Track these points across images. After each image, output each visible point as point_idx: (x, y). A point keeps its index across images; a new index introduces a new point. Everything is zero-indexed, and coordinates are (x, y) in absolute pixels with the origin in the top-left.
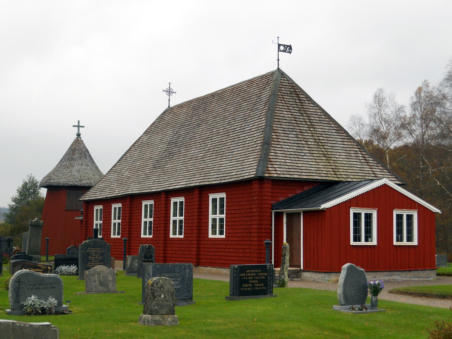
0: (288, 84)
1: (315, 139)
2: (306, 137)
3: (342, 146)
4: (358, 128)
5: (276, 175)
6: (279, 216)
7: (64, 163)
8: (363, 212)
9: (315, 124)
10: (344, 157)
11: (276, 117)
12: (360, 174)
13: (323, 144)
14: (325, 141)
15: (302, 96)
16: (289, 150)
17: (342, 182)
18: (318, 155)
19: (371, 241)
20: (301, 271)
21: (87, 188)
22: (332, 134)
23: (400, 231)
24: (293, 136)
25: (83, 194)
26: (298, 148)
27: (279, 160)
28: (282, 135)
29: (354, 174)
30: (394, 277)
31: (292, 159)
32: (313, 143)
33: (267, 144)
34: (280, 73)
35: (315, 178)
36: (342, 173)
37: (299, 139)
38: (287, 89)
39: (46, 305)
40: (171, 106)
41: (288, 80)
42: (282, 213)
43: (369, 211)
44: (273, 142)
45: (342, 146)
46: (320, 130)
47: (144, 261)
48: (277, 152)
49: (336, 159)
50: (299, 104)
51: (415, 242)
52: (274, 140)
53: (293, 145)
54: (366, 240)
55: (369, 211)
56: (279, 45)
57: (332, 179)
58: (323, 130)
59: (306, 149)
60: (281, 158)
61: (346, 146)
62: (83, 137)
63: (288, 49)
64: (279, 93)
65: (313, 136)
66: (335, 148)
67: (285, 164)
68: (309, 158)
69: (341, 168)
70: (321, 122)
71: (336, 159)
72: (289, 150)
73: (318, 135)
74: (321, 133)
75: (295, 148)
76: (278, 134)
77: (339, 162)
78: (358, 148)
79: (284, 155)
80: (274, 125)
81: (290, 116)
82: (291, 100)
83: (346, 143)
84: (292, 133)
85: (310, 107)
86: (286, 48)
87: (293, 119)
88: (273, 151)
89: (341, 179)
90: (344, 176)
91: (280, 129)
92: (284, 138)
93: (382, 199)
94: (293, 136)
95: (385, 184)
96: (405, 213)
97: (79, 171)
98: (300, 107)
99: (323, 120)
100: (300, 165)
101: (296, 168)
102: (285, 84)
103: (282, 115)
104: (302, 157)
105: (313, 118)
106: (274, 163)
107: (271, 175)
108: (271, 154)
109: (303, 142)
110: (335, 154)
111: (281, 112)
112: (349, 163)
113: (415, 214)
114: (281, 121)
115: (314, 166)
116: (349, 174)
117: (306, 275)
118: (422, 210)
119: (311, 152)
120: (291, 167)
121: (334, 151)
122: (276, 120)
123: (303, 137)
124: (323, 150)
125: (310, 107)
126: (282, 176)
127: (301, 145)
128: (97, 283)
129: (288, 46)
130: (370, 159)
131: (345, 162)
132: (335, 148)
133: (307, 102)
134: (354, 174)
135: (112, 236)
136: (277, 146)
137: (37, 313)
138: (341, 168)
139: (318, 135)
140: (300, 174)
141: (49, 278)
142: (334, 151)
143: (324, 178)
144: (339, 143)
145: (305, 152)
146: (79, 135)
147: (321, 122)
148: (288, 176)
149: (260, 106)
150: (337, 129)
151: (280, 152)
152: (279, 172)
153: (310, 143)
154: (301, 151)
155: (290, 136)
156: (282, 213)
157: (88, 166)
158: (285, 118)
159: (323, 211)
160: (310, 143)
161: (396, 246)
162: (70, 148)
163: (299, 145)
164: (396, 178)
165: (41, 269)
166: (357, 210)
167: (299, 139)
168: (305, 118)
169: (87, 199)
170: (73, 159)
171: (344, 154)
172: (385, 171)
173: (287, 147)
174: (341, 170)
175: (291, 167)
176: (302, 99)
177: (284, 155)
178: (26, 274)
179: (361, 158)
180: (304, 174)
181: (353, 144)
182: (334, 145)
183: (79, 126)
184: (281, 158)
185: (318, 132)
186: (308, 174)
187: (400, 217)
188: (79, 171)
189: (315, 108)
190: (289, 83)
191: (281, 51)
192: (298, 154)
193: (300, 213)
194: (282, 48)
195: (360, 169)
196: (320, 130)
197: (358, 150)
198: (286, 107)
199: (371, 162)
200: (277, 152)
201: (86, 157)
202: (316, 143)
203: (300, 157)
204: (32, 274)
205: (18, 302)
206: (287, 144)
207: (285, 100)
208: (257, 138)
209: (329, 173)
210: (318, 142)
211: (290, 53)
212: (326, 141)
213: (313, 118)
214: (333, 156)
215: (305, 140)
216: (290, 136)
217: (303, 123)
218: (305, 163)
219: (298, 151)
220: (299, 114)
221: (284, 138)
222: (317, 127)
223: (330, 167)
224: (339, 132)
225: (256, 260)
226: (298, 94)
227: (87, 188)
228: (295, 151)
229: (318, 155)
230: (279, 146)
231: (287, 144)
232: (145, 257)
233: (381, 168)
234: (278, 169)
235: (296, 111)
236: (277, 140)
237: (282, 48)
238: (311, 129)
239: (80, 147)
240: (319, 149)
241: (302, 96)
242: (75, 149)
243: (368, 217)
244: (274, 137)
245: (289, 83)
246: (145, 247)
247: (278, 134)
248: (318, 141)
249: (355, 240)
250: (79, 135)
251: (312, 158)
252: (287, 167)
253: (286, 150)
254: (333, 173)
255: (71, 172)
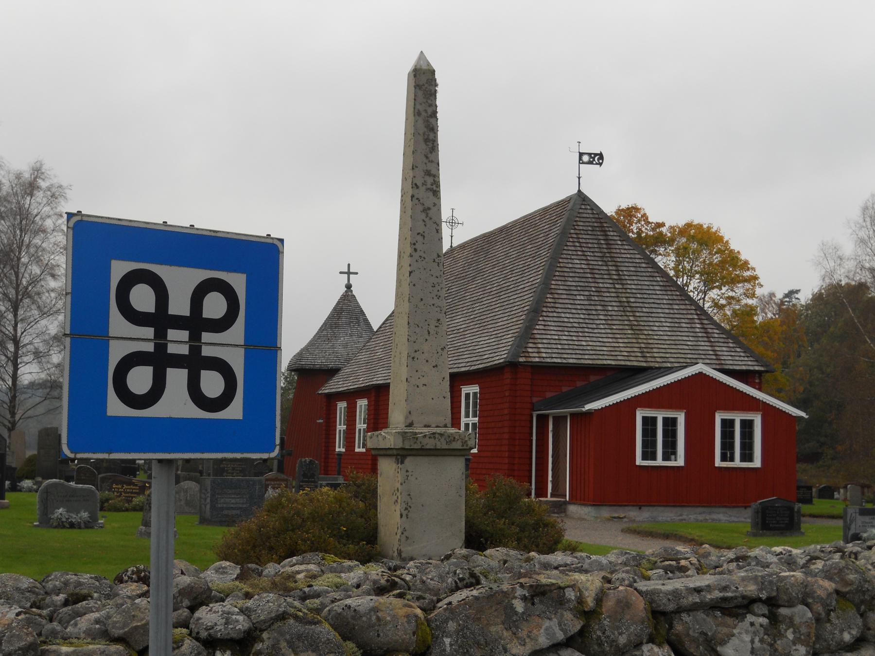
0: (591, 216)
1: (620, 302)
2: (606, 299)
3: (667, 311)
4: (832, 264)
5: (537, 360)
6: (543, 420)
7: (325, 333)
8: (660, 416)
9: (627, 277)
10: (667, 329)
11: (558, 269)
12: (689, 356)
13: (635, 309)
14: (638, 305)
15: (612, 234)
16: (571, 320)
17: (651, 368)
18: (621, 327)
19: (676, 460)
20: (565, 503)
21: (333, 372)
22: (654, 292)
23: (728, 446)
24: (582, 298)
25: (326, 381)
26: (587, 317)
27: (549, 337)
28: (565, 296)
29: (679, 355)
30: (715, 516)
31: (572, 334)
32: (616, 309)
33: (536, 311)
34: (581, 198)
35: (605, 362)
36: (656, 355)
37: (592, 303)
38: (587, 224)
39: (74, 518)
40: (454, 245)
41: (592, 209)
42: (546, 417)
43: (670, 414)
44: (545, 309)
45: (667, 311)
46: (633, 287)
47: (303, 482)
48: (549, 323)
49: (650, 333)
50: (605, 246)
51: (757, 463)
52: (548, 305)
53: (579, 312)
54: (666, 458)
55: (670, 414)
56: (581, 155)
57: (635, 364)
58: (640, 287)
59: (602, 317)
60: (553, 332)
61: (676, 311)
62: (355, 291)
63: (597, 158)
64: (572, 231)
65: (618, 297)
66: (653, 315)
67: (557, 342)
68: (603, 331)
69: (656, 346)
70: (639, 274)
71: (650, 333)
72: (571, 320)
73: (628, 295)
74: (634, 291)
75: (582, 316)
76: (556, 296)
77: (656, 337)
78: (697, 314)
79: (560, 329)
80: (553, 282)
81: (583, 266)
82: (591, 241)
83: (676, 307)
84: (582, 293)
85: (623, 251)
86: (594, 159)
87: (588, 271)
88: (543, 323)
89: (652, 365)
90: (658, 360)
91: (561, 287)
92: (567, 301)
93: (699, 397)
94: (582, 298)
95: (701, 373)
96: (738, 417)
97: (345, 346)
98: (606, 251)
99: (643, 270)
100: (584, 343)
101: (576, 347)
102: (585, 215)
103: (570, 266)
104: (590, 330)
105: (624, 269)
106: (539, 341)
107: (530, 360)
108: (537, 327)
109: (599, 308)
110: (651, 324)
111: (570, 261)
112: (673, 338)
113: (757, 420)
114: (566, 274)
115: (608, 344)
116: (668, 355)
117: (572, 509)
118: (769, 413)
119: (610, 322)
120: (566, 347)
121: (651, 319)
122: (557, 273)
123: (601, 298)
124: (631, 318)
125: (623, 251)
126: (549, 360)
127: (594, 312)
128: (183, 503)
129: (596, 155)
130: (715, 331)
131: (666, 338)
132: (653, 315)
133: (619, 242)
134: (679, 355)
135: (357, 450)
136: (551, 314)
137: (64, 527)
138: (656, 346)
139: (628, 295)
140: (580, 357)
141: (81, 489)
142: (651, 319)
143: (623, 363)
144: (663, 306)
145: (598, 322)
146: (349, 287)
147: (639, 274)
148: (559, 361)
149: (543, 252)
150: (665, 284)
151: (553, 324)
152: (544, 355)
153: (610, 308)
154: (591, 322)
155: (578, 297)
156: (546, 417)
157: (361, 337)
158: (573, 270)
159: (589, 413)
160: (610, 308)
161: (720, 468)
162: (335, 309)
163: (590, 312)
164: (757, 361)
165: (136, 485)
166: (650, 413)
167: (592, 303)
168: (610, 268)
169: (326, 391)
170: (337, 326)
171: (668, 324)
172: (738, 350)
173: (568, 315)
174: (655, 350)
175: (566, 347)
176: (610, 238)
177: (560, 329)
178: (55, 484)
179: (698, 330)
180: (586, 357)
181: (689, 307)
182: (654, 310)
183: (349, 273)
184: (553, 332)
185: (628, 291)
186: (594, 357)
187: (728, 425)
188: (345, 346)
189: (631, 252)
190: (593, 214)
191: (583, 163)
192: (585, 325)
193: (566, 417)
194: (586, 158)
195: (691, 348)
196: (633, 287)
197: (696, 317)
198: (579, 253)
199: (716, 335)
200: (549, 323)
201: (358, 323)
202: (622, 309)
203: (586, 330)
204: (62, 484)
205: (46, 515)
206: (568, 311)
207: (581, 240)
208: (523, 301)
209: (632, 354)
210: (625, 307)
211: (601, 164)
212: (641, 305)
213: (624, 269)
214: (647, 328)
215: (602, 303)
216: (578, 297)
217: (605, 277)
218: (595, 339)
219: (587, 321)
220: (600, 263)
221: (567, 301)
222: (629, 282)
223: (637, 345)
224: (668, 288)
225: (527, 484)
226: (605, 231)
227: (333, 372)
228: (581, 321)
229: (621, 327)
230: (555, 314)
231: (568, 311)
232: (305, 475)
233: (731, 345)
234: (543, 350)
235: (597, 259)
236: (552, 305)
237: (586, 158)
238: (617, 286)
239: (350, 306)
240: (625, 318)
241: (612, 234)
242: (342, 310)
243: (670, 424)
244: (550, 300)
245: (593, 214)
246: (305, 461)
247: (556, 296)
248: (626, 304)
249: (645, 457)
250: (349, 287)
251: (609, 331)
252: (559, 347)
253: (566, 320)
254: (639, 354)
255: (333, 347)
